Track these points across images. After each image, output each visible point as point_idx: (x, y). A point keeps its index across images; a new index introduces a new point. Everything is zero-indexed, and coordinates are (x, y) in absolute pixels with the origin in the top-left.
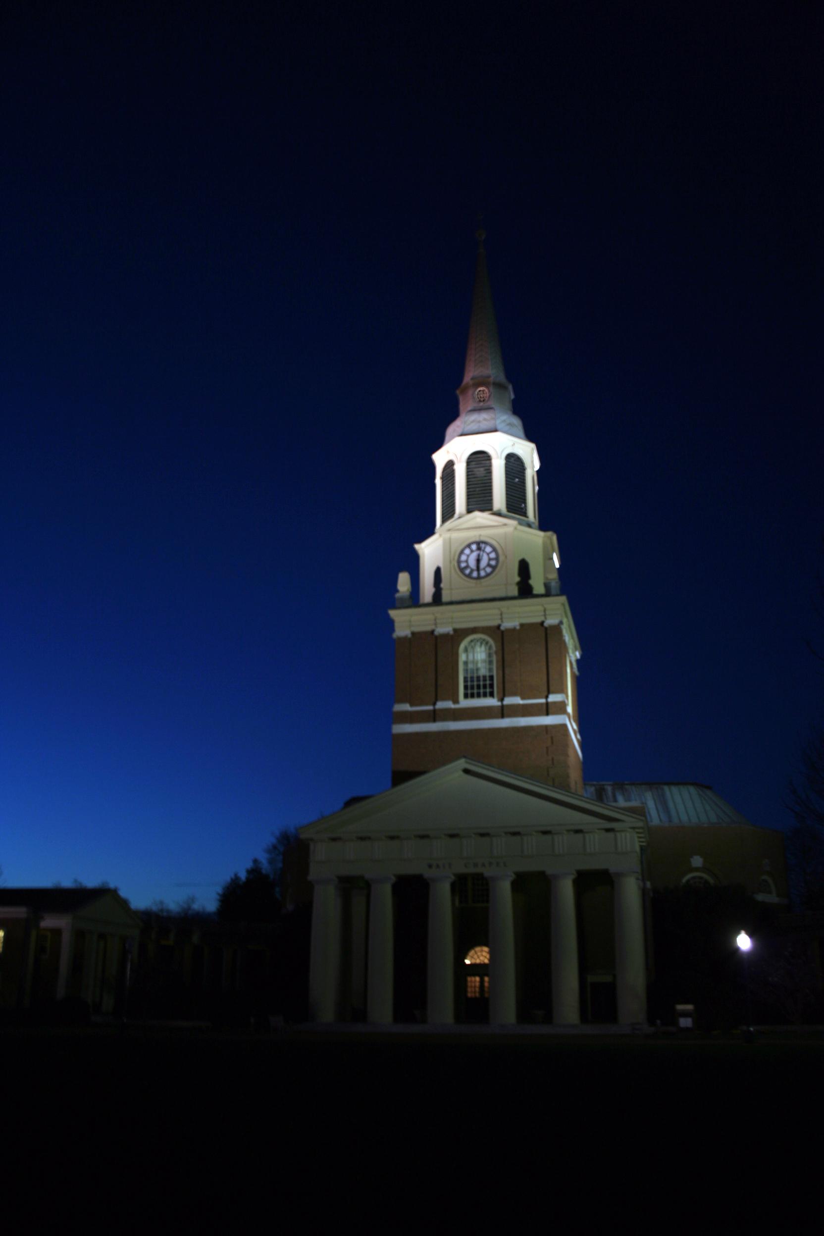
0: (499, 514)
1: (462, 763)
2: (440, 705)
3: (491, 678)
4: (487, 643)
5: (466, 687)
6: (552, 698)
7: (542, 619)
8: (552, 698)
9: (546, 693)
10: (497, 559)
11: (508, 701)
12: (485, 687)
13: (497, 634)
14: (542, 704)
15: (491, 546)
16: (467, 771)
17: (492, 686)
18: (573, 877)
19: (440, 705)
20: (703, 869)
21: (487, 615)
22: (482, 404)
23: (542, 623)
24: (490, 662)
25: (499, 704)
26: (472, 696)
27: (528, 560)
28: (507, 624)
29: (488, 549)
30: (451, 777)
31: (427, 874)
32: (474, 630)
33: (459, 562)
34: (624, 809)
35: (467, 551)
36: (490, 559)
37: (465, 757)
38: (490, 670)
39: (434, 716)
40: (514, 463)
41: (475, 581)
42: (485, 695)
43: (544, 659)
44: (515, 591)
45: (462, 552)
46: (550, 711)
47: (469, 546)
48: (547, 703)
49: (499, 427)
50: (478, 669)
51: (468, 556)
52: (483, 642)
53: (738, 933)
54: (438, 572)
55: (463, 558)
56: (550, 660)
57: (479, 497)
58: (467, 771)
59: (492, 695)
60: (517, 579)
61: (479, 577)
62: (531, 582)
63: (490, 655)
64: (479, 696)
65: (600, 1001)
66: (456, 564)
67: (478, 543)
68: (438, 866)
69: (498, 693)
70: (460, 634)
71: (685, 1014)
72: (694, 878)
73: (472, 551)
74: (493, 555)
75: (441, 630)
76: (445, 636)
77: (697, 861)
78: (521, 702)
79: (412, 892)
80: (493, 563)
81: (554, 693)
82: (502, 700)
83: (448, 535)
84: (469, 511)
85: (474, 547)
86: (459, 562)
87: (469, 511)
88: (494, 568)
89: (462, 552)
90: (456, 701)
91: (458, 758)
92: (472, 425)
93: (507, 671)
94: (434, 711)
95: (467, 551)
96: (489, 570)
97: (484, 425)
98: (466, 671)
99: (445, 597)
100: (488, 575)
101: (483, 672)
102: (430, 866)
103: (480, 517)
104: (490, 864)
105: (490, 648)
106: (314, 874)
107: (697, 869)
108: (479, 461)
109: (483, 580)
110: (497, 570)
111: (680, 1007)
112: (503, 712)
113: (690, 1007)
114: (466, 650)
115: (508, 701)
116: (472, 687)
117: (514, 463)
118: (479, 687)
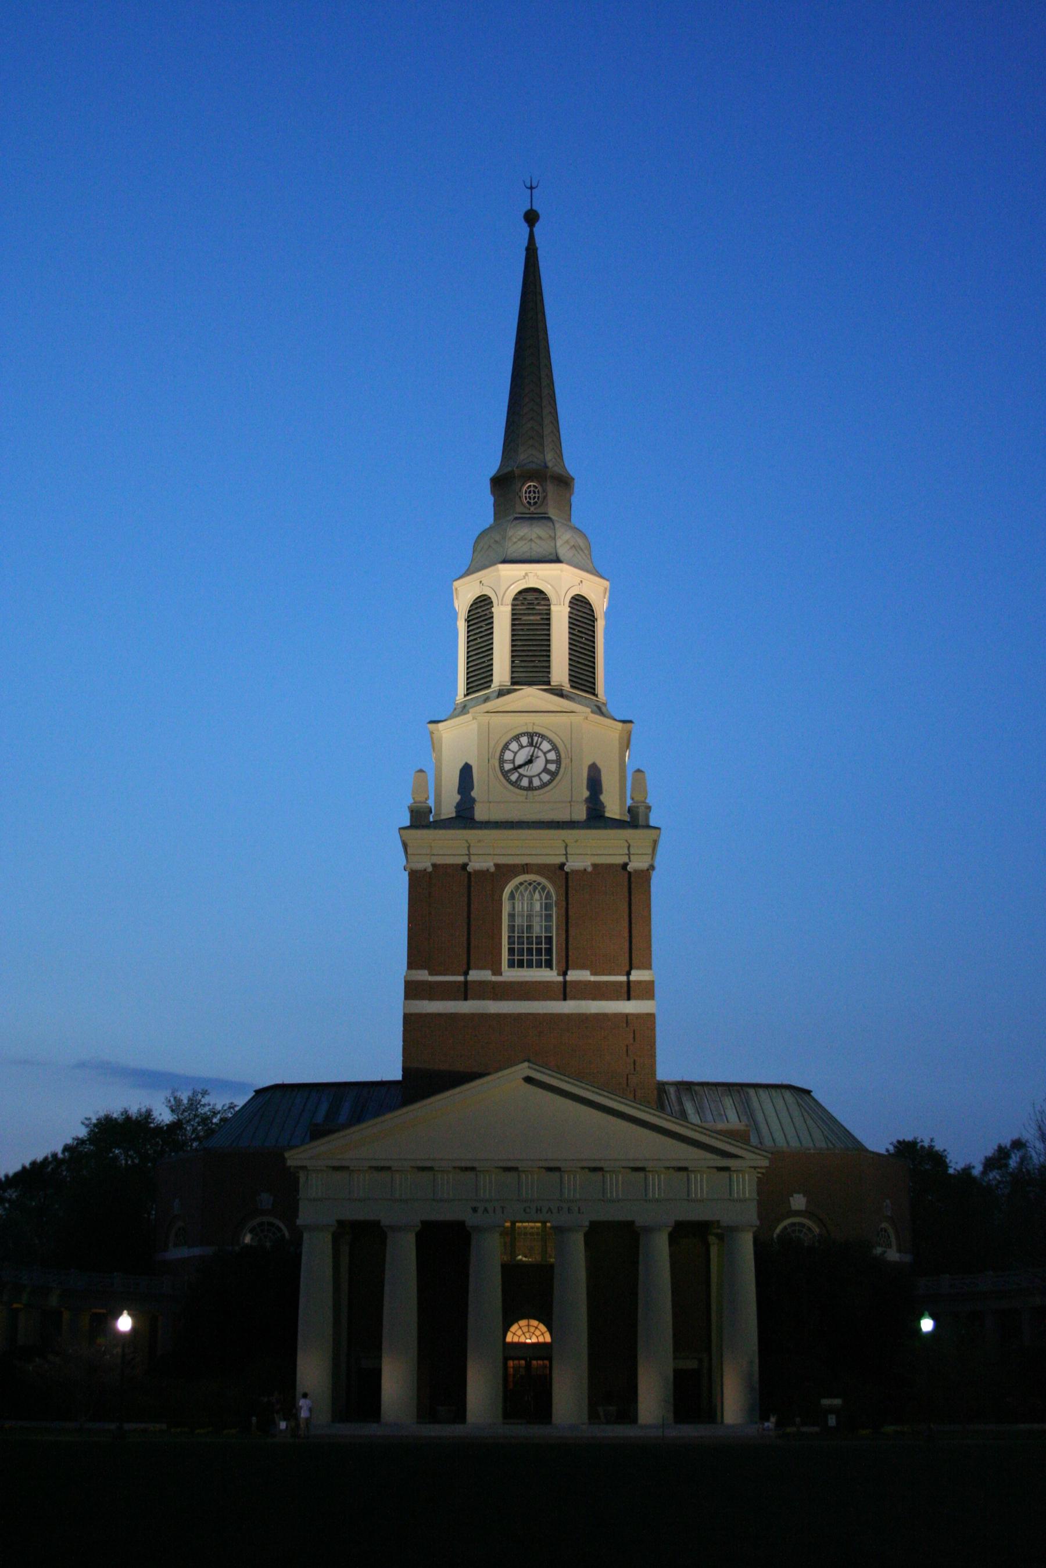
0: (559, 693)
1: (524, 1069)
2: (474, 975)
3: (549, 939)
4: (544, 888)
5: (511, 951)
6: (636, 975)
7: (625, 859)
8: (636, 975)
9: (627, 968)
10: (558, 762)
11: (573, 975)
12: (539, 952)
13: (559, 873)
14: (621, 982)
15: (550, 741)
16: (528, 1080)
17: (549, 951)
18: (670, 1229)
19: (474, 975)
20: (807, 1213)
21: (545, 849)
22: (532, 509)
23: (625, 866)
24: (548, 917)
25: (561, 979)
26: (521, 964)
27: (600, 764)
28: (574, 864)
29: (546, 746)
30: (505, 1090)
31: (470, 1219)
32: (526, 868)
33: (502, 761)
34: (720, 1132)
35: (514, 746)
36: (547, 761)
37: (529, 1061)
38: (548, 929)
39: (465, 991)
40: (580, 606)
41: (525, 792)
42: (539, 965)
43: (626, 917)
44: (581, 813)
45: (506, 747)
46: (632, 993)
47: (517, 738)
48: (629, 982)
49: (563, 552)
50: (530, 927)
51: (515, 753)
52: (536, 886)
53: (120, 1314)
54: (466, 772)
55: (508, 756)
56: (633, 921)
57: (531, 665)
58: (528, 1080)
59: (549, 965)
60: (586, 794)
61: (530, 788)
62: (603, 798)
63: (548, 907)
64: (530, 965)
65: (693, 1396)
66: (497, 764)
67: (531, 735)
68: (486, 1210)
69: (558, 962)
70: (505, 872)
71: (831, 1410)
72: (793, 1224)
73: (522, 747)
74: (552, 756)
75: (476, 864)
76: (483, 874)
77: (798, 1202)
78: (593, 978)
79: (445, 1247)
80: (552, 767)
81: (639, 968)
82: (565, 974)
83: (486, 718)
84: (517, 681)
85: (524, 740)
86: (502, 761)
87: (517, 681)
88: (554, 775)
89: (506, 747)
90: (498, 972)
91: (510, 1063)
92: (521, 543)
93: (572, 932)
94: (466, 983)
95: (514, 746)
96: (546, 777)
97: (540, 548)
98: (512, 928)
99: (480, 813)
100: (544, 785)
101: (537, 930)
102: (475, 1210)
103: (531, 696)
104: (560, 1209)
105: (548, 896)
106: (305, 1216)
107: (798, 1213)
108: (531, 604)
109: (536, 793)
110: (558, 778)
111: (826, 1402)
112: (565, 991)
113: (838, 1402)
114: (512, 896)
115: (573, 975)
116: (521, 952)
117: (580, 606)
118: (530, 951)
